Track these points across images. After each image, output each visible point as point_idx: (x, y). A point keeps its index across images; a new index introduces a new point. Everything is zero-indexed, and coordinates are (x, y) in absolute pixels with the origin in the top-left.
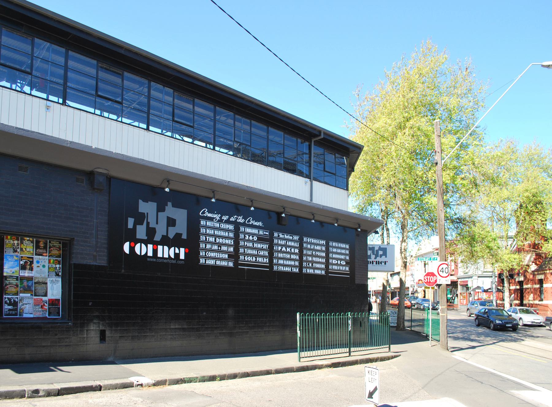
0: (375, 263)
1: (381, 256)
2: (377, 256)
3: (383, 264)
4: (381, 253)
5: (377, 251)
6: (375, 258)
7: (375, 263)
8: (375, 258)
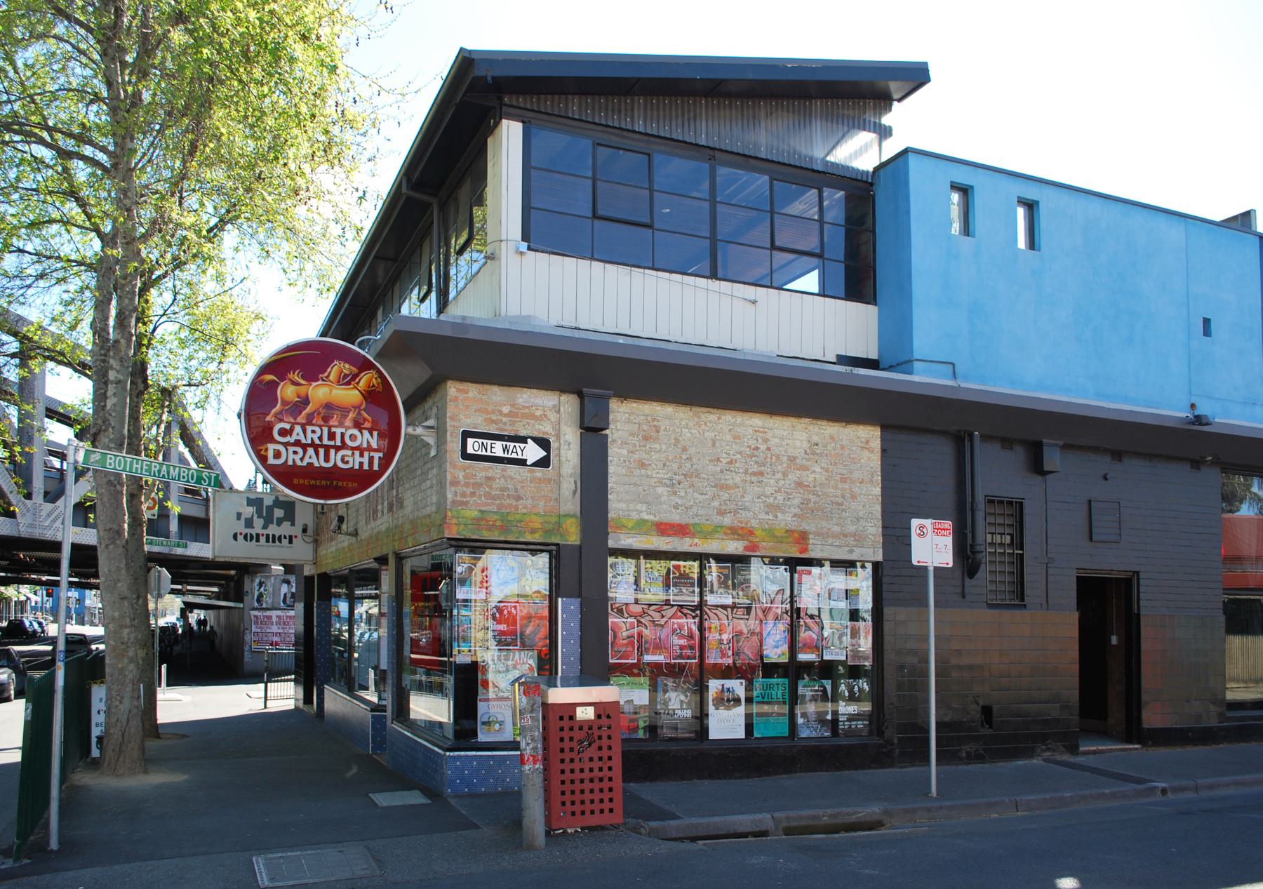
0: (263, 539)
1: (279, 523)
2: (268, 521)
3: (285, 542)
4: (279, 513)
5: (270, 509)
6: (265, 527)
7: (263, 539)
8: (265, 527)
